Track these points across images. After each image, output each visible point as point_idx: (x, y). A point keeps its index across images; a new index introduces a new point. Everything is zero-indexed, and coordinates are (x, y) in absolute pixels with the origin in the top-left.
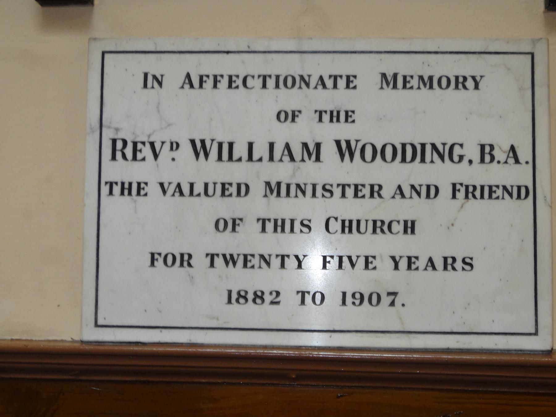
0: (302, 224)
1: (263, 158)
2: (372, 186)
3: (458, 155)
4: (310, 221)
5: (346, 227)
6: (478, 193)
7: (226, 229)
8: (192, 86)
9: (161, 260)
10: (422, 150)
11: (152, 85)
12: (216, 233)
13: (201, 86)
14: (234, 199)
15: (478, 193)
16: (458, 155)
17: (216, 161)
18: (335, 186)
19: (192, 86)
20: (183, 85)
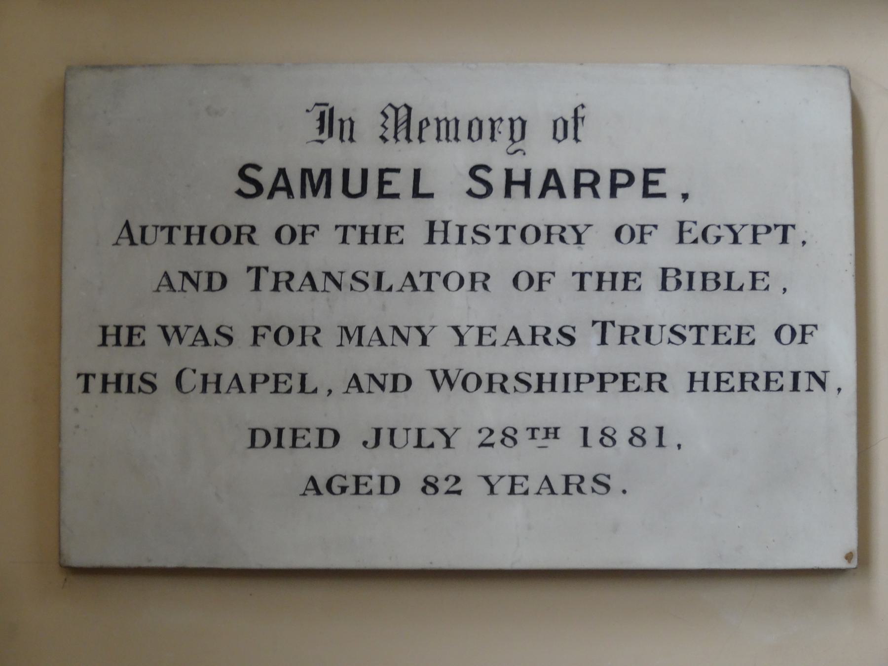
0: (142, 379)
1: (437, 391)
2: (743, 375)
3: (201, 374)
4: (155, 375)
5: (113, 383)
6: (761, 383)
7: (295, 239)
8: (241, 391)
9: (270, 336)
10: (321, 184)
11: (808, 387)
12: (582, 249)
13: (254, 390)
14: (642, 395)
15: (761, 383)
16: (201, 374)
17: (100, 393)
18: (493, 228)
19: (241, 391)
20: (229, 389)
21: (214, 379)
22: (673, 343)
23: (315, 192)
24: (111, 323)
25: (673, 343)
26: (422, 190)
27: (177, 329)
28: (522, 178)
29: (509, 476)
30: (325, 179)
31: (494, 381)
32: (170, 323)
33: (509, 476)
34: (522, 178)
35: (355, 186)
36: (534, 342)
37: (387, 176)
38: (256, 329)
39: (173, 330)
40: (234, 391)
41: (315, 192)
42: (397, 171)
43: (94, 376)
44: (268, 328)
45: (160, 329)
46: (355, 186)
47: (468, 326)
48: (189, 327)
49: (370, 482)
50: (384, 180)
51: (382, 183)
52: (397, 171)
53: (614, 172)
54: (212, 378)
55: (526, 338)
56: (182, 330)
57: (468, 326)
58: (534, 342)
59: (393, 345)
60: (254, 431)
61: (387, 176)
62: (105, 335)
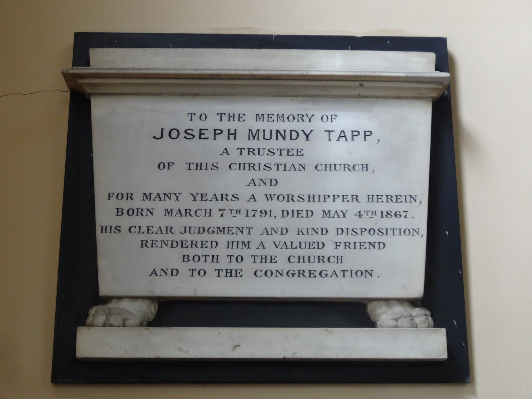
19: (181, 215)
21: (209, 211)
22: (233, 200)
23: (254, 138)
24: (371, 194)
25: (233, 200)
26: (292, 138)
27: (270, 195)
28: (233, 132)
29: (378, 242)
30: (257, 134)
31: (187, 212)
32: (268, 193)
33: (378, 242)
34: (233, 132)
35: (268, 136)
36: (222, 200)
37: (203, 132)
38: (109, 194)
39: (269, 196)
40: (336, 216)
41: (254, 138)
42: (207, 130)
43: (369, 211)
44: (114, 194)
45: (265, 195)
46: (268, 136)
47: (196, 194)
48: (197, 194)
49: (365, 245)
50: (216, 133)
51: (201, 134)
52: (207, 130)
53: (365, 132)
54: (208, 211)
55: (219, 198)
56: (272, 196)
57: (196, 194)
58: (222, 200)
59: (164, 200)
60: (337, 229)
61: (203, 132)
62: (369, 198)
